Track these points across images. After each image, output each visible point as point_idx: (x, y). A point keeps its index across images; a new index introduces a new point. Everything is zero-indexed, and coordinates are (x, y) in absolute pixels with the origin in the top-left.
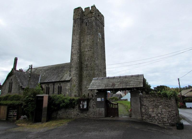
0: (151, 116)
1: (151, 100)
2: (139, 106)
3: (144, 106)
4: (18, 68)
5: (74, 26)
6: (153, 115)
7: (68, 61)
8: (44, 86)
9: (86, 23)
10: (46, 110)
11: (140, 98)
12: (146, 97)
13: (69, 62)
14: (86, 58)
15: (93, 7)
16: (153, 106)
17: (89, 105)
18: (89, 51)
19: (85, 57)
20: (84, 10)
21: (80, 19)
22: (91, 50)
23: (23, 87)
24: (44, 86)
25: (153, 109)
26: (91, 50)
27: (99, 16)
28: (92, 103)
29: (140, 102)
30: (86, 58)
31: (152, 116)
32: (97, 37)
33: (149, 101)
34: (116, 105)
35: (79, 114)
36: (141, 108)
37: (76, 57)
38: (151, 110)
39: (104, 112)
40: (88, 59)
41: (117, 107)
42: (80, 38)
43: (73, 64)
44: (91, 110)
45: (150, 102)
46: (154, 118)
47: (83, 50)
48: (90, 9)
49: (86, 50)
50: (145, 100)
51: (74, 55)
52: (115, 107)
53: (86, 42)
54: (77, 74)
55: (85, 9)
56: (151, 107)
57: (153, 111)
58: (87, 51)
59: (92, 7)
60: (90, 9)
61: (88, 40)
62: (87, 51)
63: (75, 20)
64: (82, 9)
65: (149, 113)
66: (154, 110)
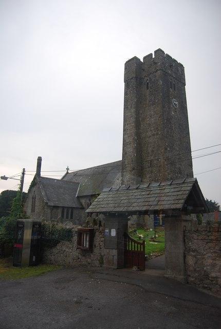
0: (207, 275)
1: (210, 238)
2: (182, 251)
3: (193, 251)
4: (43, 174)
5: (126, 94)
6: (213, 275)
7: (119, 157)
8: (83, 201)
9: (148, 83)
10: (30, 246)
11: (184, 231)
12: (197, 230)
13: (120, 158)
14: (150, 149)
15: (159, 52)
16: (215, 252)
17: (95, 243)
18: (154, 135)
19: (148, 147)
20: (142, 60)
21: (136, 78)
22: (157, 134)
23: (49, 204)
24: (83, 201)
25: (214, 260)
26: (157, 134)
27: (171, 66)
28: (98, 239)
29: (184, 241)
30: (150, 149)
31: (210, 275)
32: (169, 108)
33: (205, 239)
34: (141, 244)
35: (80, 257)
36: (185, 257)
37: (130, 149)
38: (210, 261)
39: (116, 257)
40: (153, 151)
41: (142, 250)
42: (137, 113)
43: (126, 161)
44: (96, 250)
45: (207, 243)
46: (214, 282)
47: (143, 135)
48: (154, 57)
49: (149, 134)
50: (195, 236)
51: (128, 146)
52: (136, 250)
53: (148, 119)
54: (134, 179)
55: (145, 58)
56: (210, 255)
57: (213, 266)
58: (150, 137)
59: (156, 52)
60: (154, 57)
61: (152, 115)
62: (150, 137)
63: (127, 81)
64: (139, 60)
65: (205, 269)
66: (217, 262)
